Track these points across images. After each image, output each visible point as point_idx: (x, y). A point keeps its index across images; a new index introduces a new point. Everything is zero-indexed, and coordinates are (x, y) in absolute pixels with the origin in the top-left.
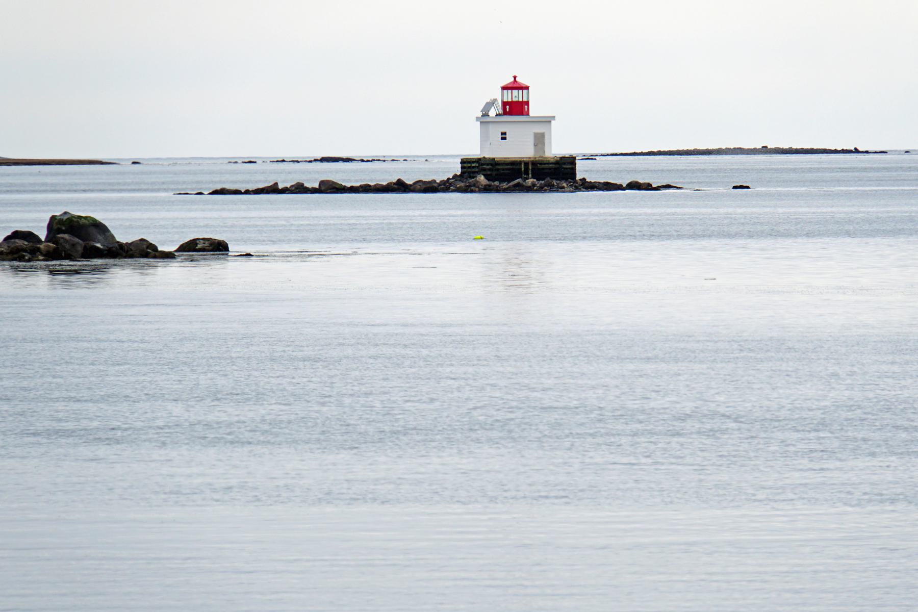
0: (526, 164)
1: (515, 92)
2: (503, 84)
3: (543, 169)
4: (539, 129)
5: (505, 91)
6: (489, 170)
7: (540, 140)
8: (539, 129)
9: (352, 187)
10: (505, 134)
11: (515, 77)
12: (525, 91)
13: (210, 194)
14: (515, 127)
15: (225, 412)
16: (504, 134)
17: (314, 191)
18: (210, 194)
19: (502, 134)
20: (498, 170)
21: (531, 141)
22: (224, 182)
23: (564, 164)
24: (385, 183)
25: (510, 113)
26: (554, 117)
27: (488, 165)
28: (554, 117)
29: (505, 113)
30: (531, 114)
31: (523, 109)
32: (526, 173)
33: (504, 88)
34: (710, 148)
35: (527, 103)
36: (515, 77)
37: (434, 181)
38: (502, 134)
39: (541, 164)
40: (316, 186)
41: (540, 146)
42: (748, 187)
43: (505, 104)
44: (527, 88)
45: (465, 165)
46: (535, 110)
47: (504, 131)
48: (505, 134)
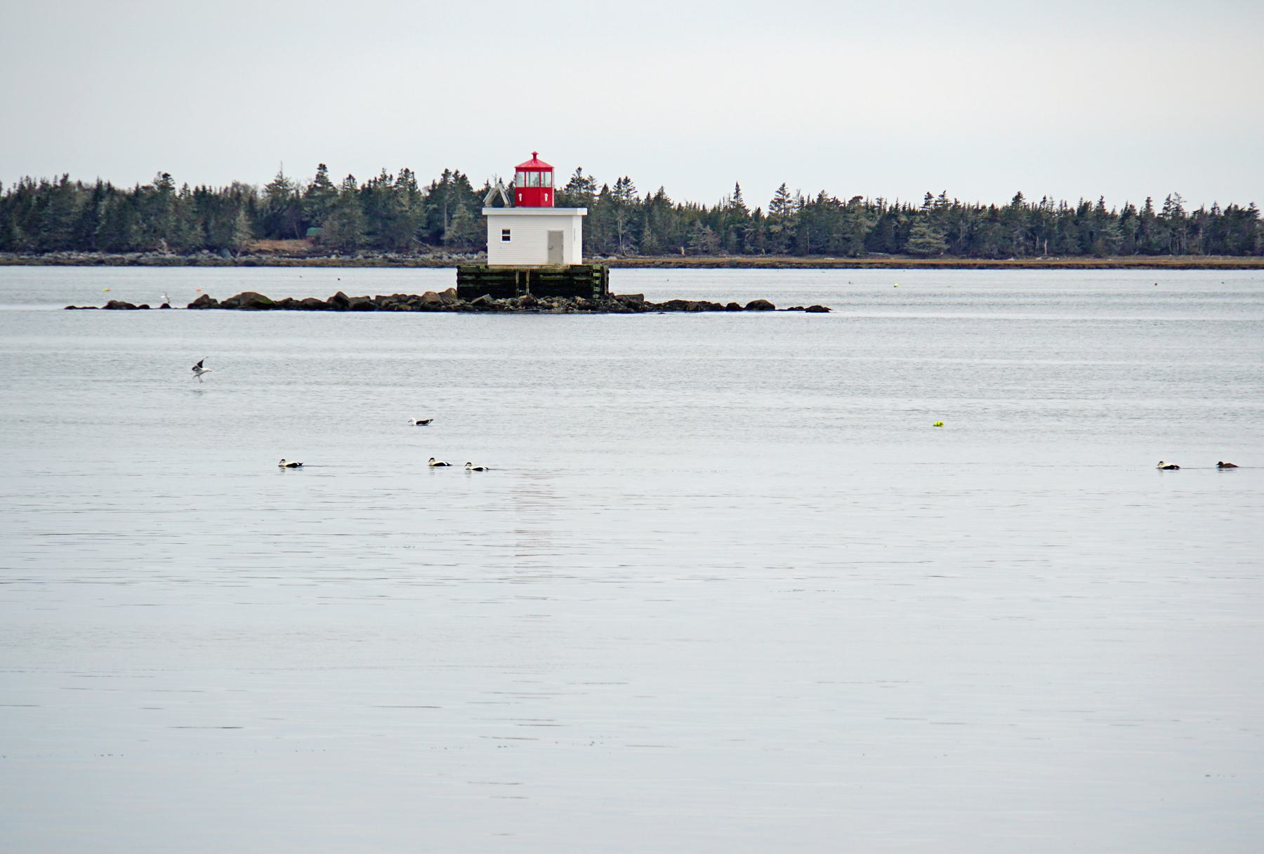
0: (522, 274)
1: (534, 175)
2: (518, 164)
3: (546, 281)
5: (522, 174)
6: (472, 281)
9: (670, 303)
10: (508, 232)
11: (535, 155)
12: (548, 174)
13: (191, 307)
17: (228, 305)
18: (191, 307)
19: (504, 232)
21: (544, 243)
22: (822, 295)
23: (577, 275)
24: (300, 299)
25: (523, 204)
27: (470, 274)
32: (522, 286)
33: (518, 169)
36: (535, 155)
38: (504, 232)
39: (544, 274)
42: (826, 310)
44: (550, 169)
47: (506, 228)
48: (508, 232)
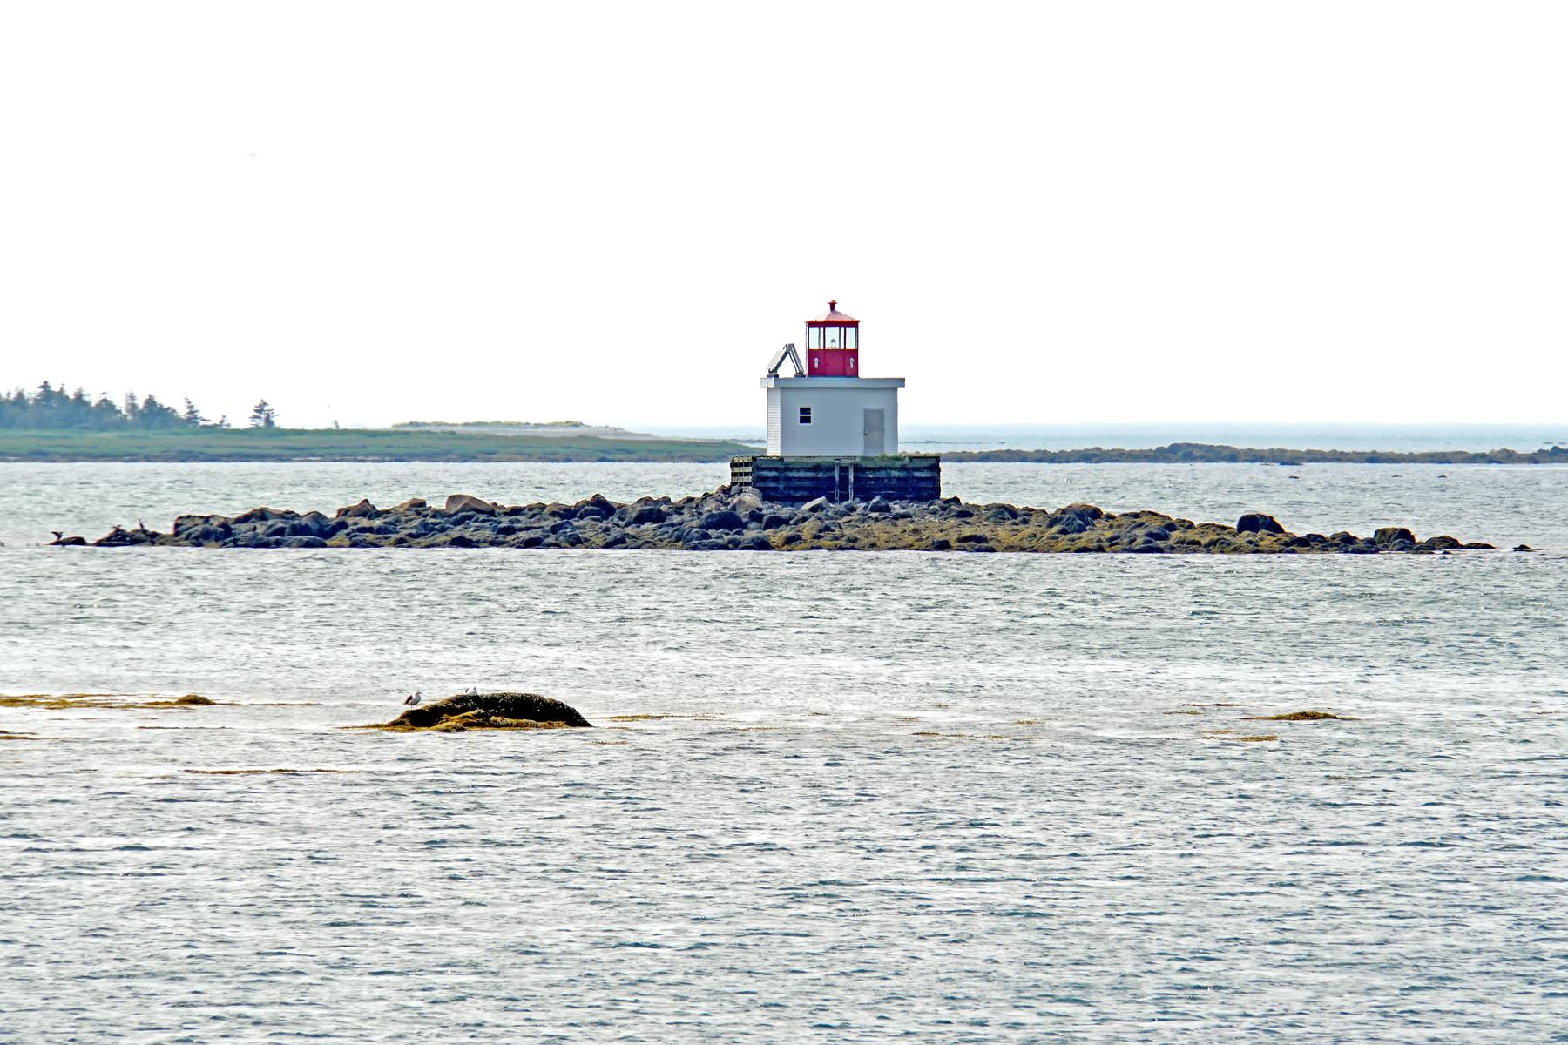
0: (844, 470)
1: (832, 333)
4: (875, 402)
5: (814, 331)
7: (881, 421)
8: (875, 402)
11: (832, 305)
12: (851, 331)
14: (826, 394)
15: (1040, 1014)
16: (805, 410)
20: (788, 479)
26: (903, 380)
28: (903, 380)
29: (813, 372)
30: (862, 374)
31: (846, 364)
34: (354, 418)
35: (854, 353)
36: (832, 305)
37: (666, 500)
40: (167, 529)
41: (875, 435)
43: (811, 354)
45: (737, 470)
46: (868, 368)
